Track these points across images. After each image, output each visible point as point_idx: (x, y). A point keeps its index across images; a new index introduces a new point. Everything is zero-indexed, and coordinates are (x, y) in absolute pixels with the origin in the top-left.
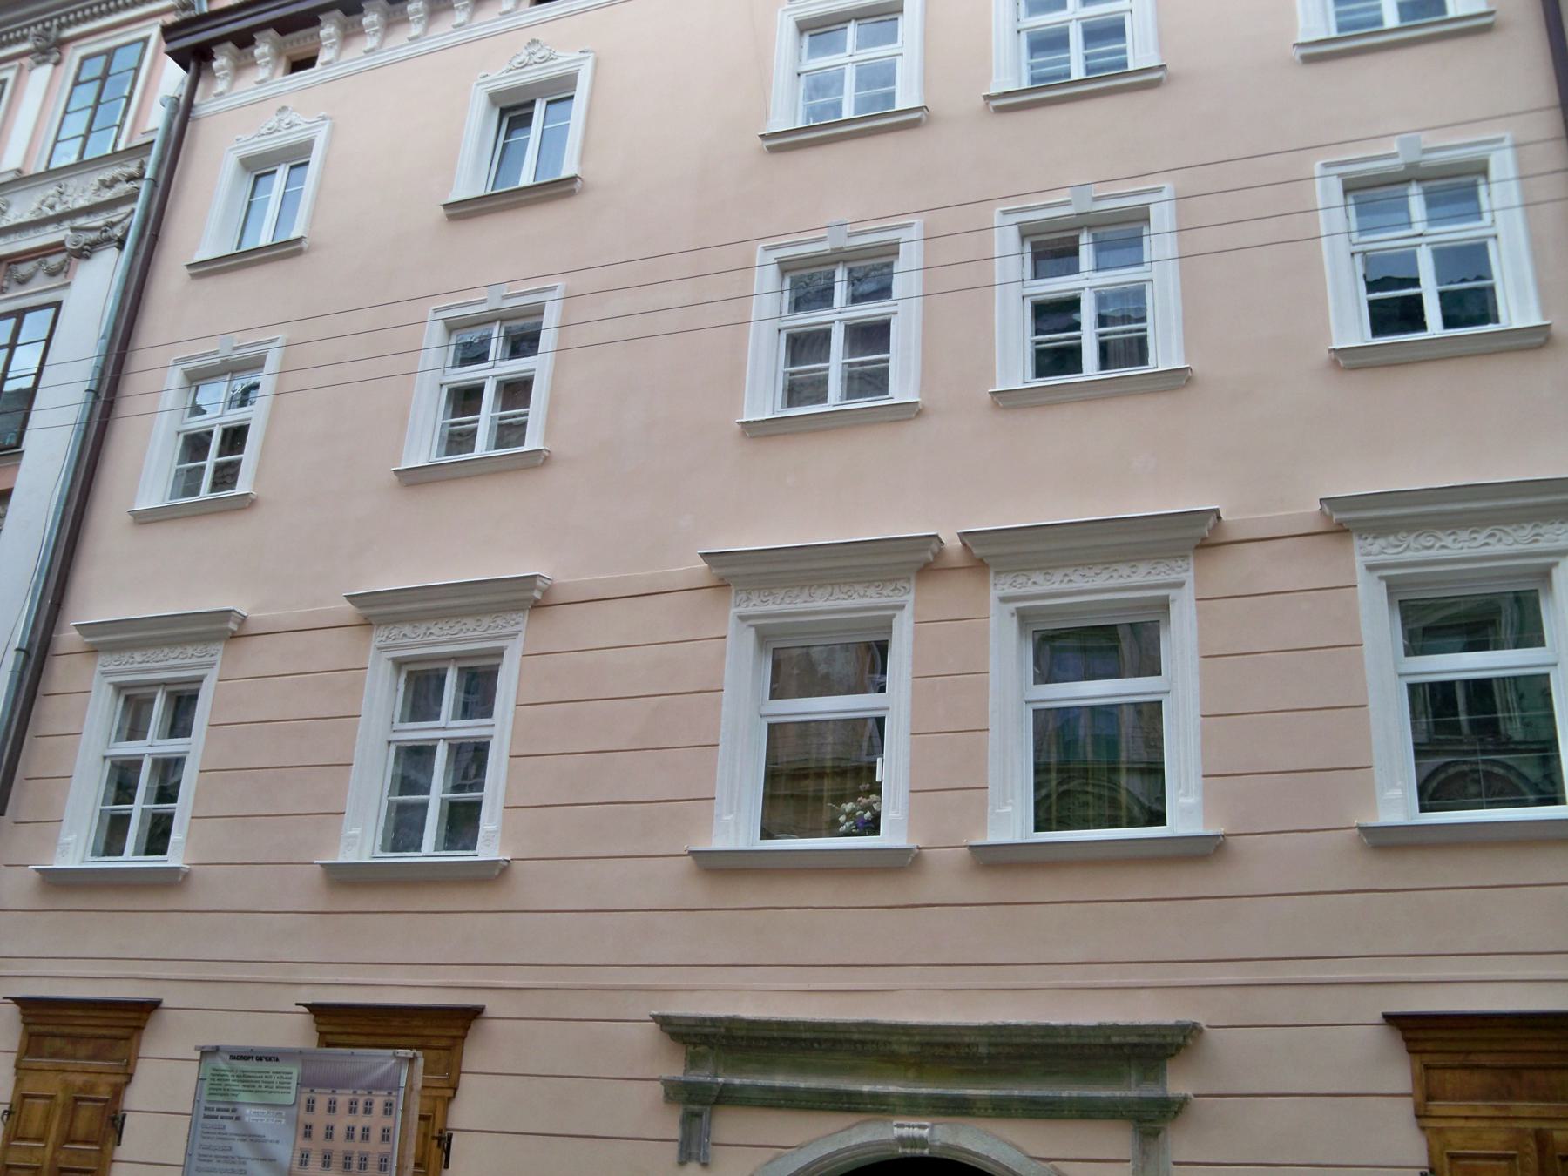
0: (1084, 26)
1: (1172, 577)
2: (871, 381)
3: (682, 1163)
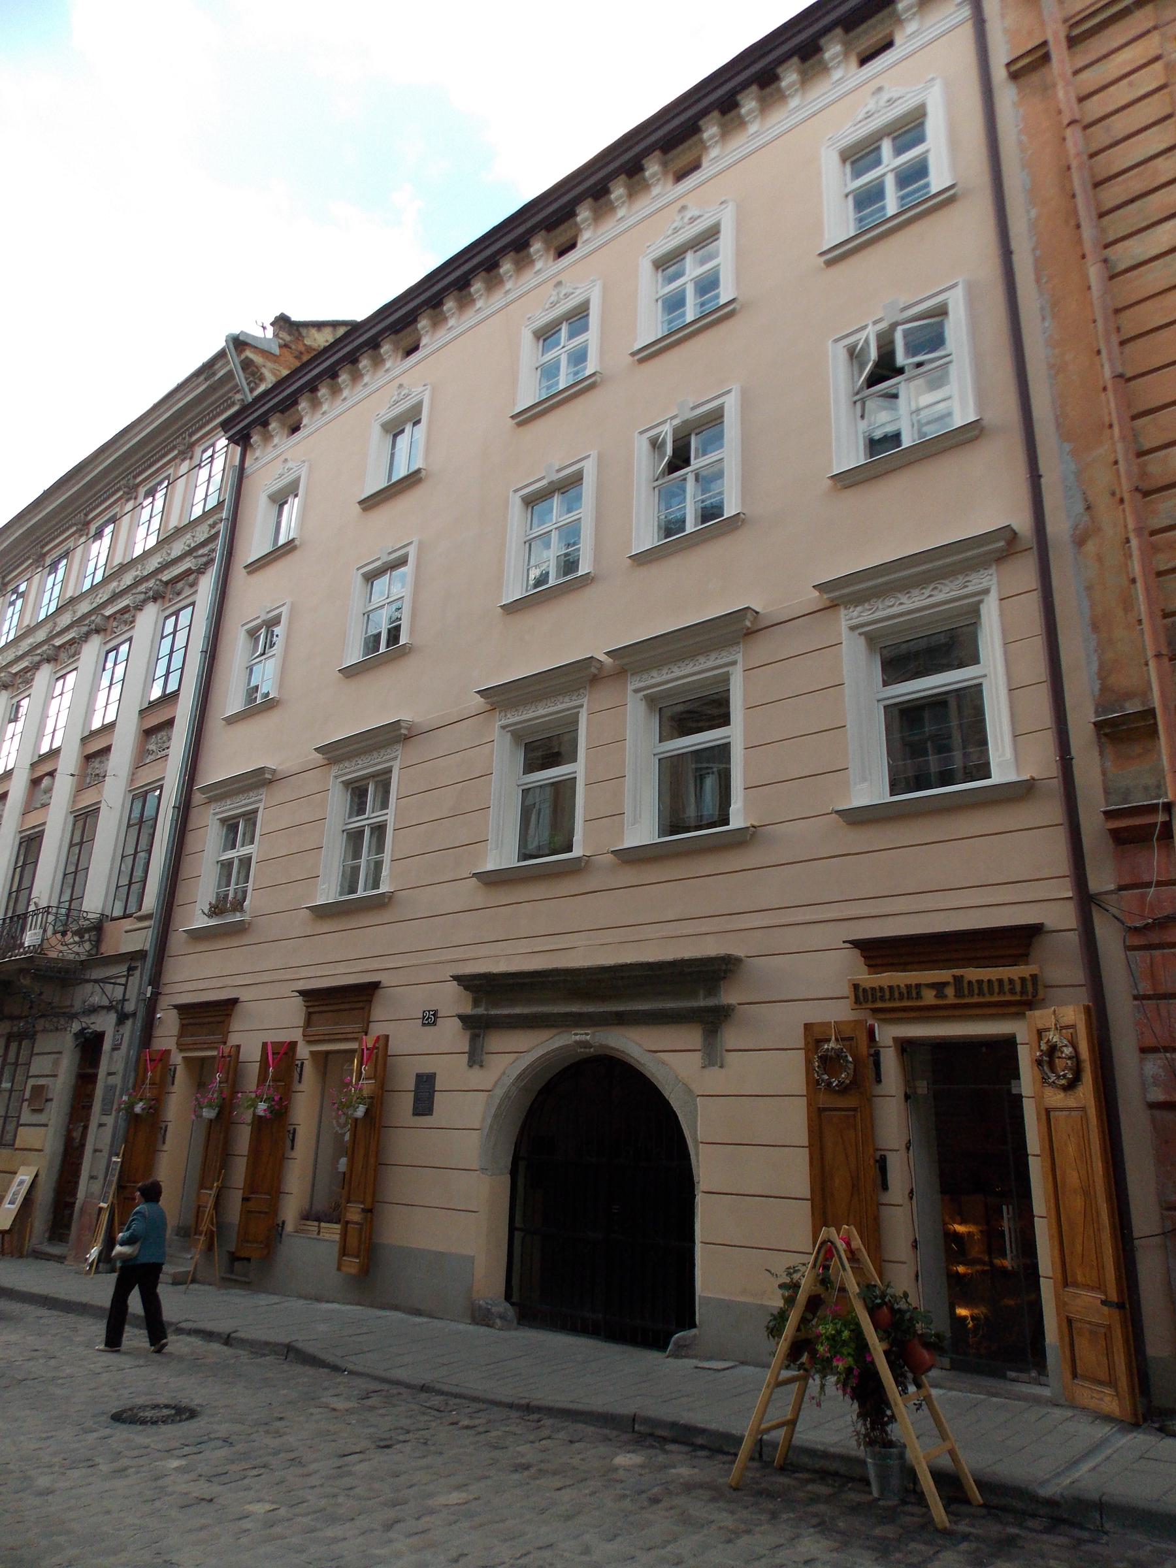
0: (696, 284)
1: (731, 658)
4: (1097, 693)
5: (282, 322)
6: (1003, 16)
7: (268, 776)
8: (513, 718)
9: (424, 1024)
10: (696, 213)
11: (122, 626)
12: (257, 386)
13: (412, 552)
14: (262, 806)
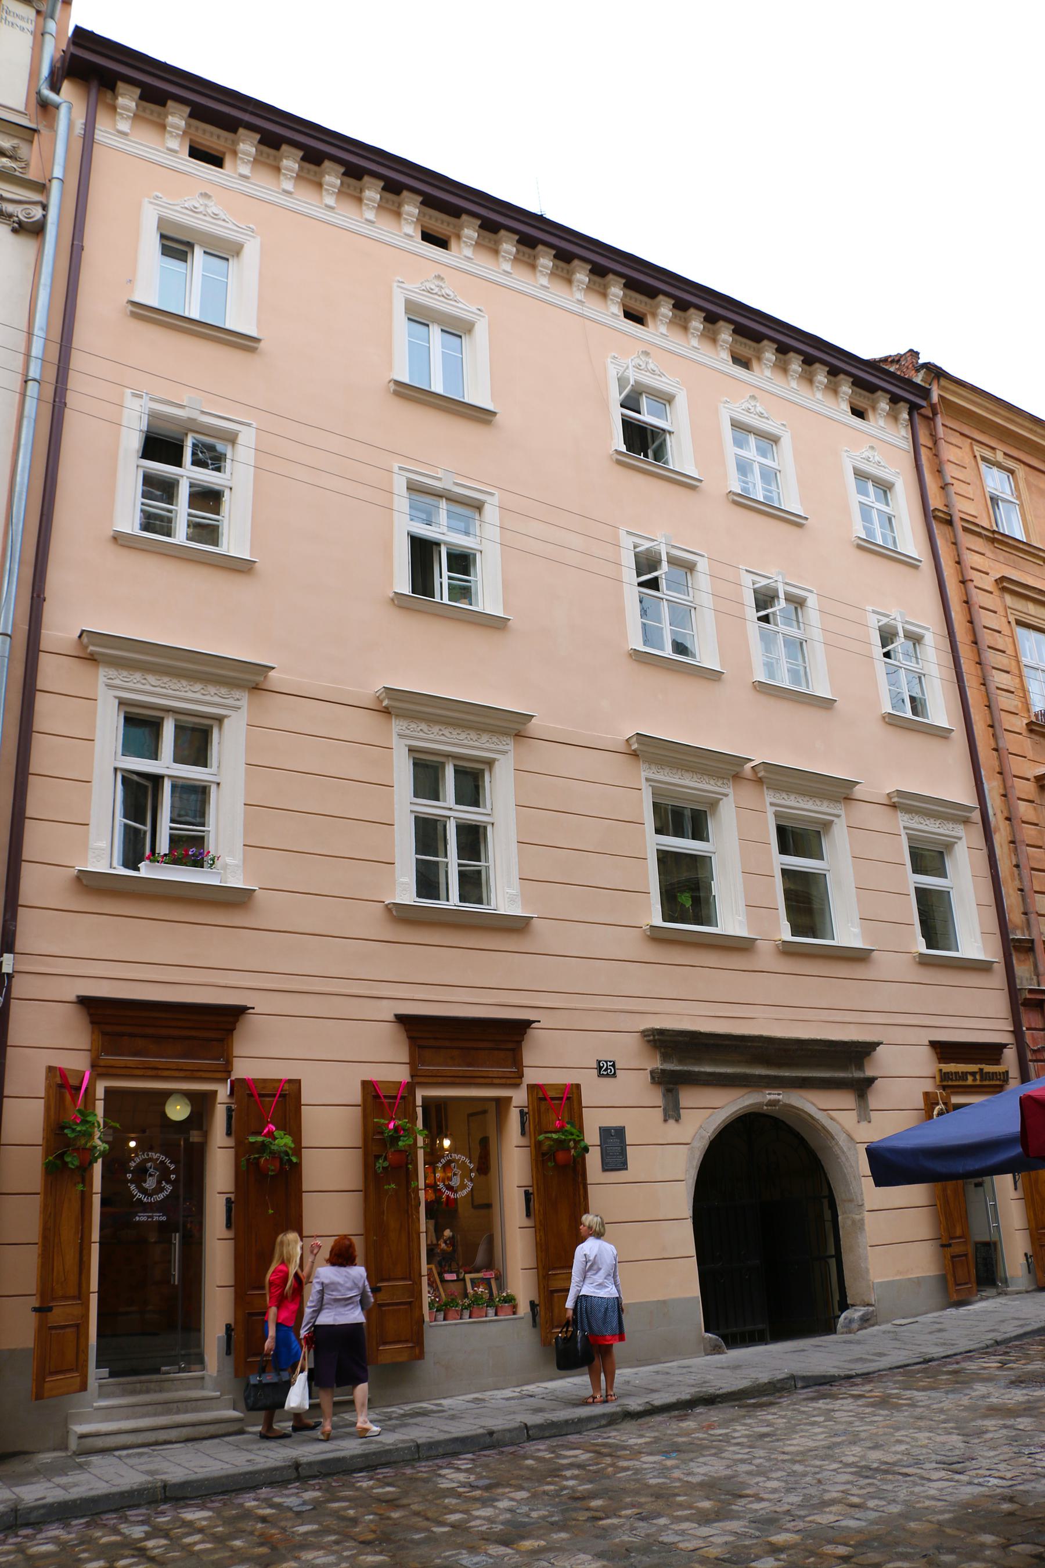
1: (836, 812)
2: (207, 533)
3: (665, 1121)
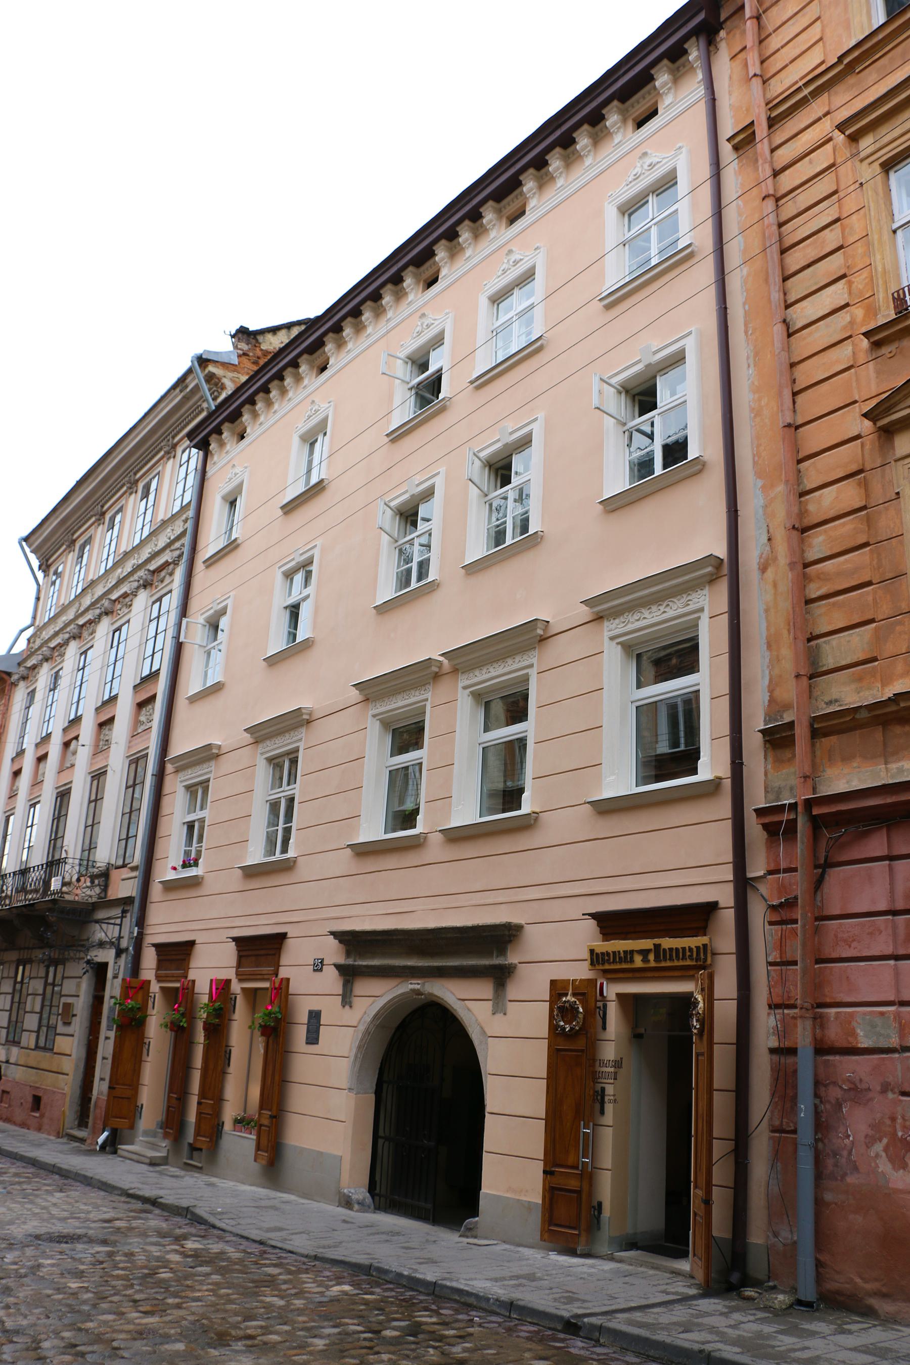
1: (526, 663)
4: (766, 703)
5: (243, 333)
6: (730, 94)
7: (215, 751)
8: (383, 707)
9: (314, 970)
10: (518, 257)
11: (124, 608)
12: (220, 394)
13: (440, 484)
14: (302, 745)
